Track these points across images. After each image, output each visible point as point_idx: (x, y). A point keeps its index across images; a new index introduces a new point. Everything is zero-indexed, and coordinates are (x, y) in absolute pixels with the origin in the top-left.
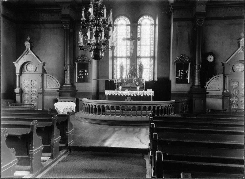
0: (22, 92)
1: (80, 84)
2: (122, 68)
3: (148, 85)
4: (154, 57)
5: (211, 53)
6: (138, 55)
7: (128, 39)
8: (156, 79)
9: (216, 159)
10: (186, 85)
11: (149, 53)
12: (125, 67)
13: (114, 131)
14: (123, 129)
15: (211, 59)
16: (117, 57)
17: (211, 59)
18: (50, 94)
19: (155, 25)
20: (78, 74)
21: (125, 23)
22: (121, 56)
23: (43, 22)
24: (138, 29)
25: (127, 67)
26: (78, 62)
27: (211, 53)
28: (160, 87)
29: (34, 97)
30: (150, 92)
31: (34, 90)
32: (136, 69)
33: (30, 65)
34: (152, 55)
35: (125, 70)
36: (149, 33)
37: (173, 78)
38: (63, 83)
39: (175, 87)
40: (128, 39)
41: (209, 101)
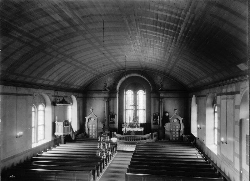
0: (89, 129)
1: (111, 125)
2: (130, 118)
3: (142, 125)
4: (145, 110)
5: (167, 112)
6: (137, 108)
7: (132, 106)
8: (146, 122)
9: (108, 120)
10: (157, 125)
11: (142, 107)
12: (131, 117)
13: (128, 146)
14: (131, 145)
15: (167, 114)
16: (127, 109)
17: (167, 114)
18: (100, 130)
19: (145, 94)
20: (111, 120)
21: (131, 93)
22: (129, 109)
23: (95, 97)
24: (137, 111)
25: (132, 119)
26: (110, 115)
27: (167, 112)
28: (147, 127)
29: (94, 131)
30: (142, 129)
31: (94, 128)
32: (136, 118)
33: (92, 118)
34: (144, 109)
35: (131, 119)
36: (142, 98)
37: (152, 122)
38: (104, 125)
39: (153, 126)
40: (132, 106)
41: (166, 132)
